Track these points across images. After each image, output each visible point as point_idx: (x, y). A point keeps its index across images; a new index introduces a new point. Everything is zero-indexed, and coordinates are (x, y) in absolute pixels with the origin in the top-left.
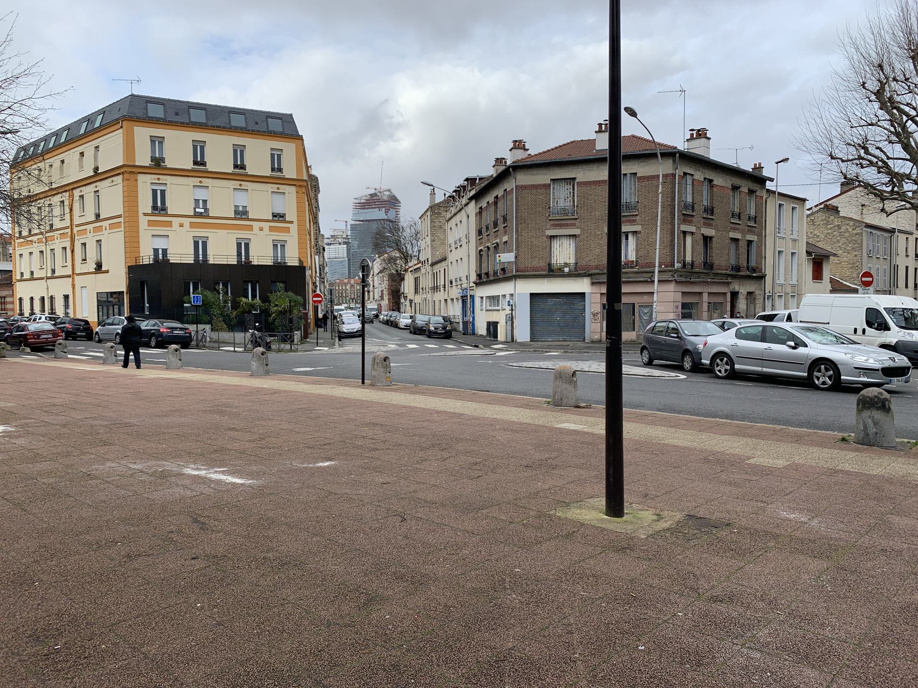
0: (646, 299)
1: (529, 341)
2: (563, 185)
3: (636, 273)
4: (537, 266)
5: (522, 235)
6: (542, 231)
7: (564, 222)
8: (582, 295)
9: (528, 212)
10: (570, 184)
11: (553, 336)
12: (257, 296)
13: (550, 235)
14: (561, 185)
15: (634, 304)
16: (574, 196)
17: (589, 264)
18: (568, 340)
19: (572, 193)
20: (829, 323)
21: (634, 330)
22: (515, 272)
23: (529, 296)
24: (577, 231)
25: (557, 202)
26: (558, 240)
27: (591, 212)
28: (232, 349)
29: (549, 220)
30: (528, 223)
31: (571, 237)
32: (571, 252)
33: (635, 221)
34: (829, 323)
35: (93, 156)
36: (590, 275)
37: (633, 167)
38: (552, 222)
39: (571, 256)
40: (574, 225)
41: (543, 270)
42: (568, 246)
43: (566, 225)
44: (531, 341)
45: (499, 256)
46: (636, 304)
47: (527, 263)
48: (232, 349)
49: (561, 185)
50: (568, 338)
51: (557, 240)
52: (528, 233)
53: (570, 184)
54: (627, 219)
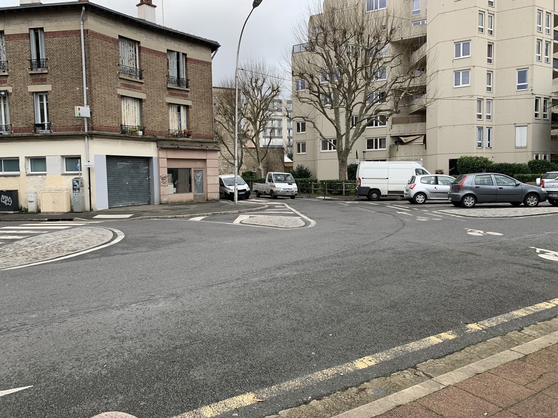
0: (199, 165)
1: (107, 208)
2: (127, 46)
3: (191, 142)
4: (111, 126)
5: (95, 89)
6: (114, 89)
7: (132, 84)
8: (148, 160)
9: (100, 64)
10: (133, 47)
11: (123, 201)
12: (431, 174)
13: (121, 94)
14: (125, 44)
15: (190, 169)
16: (136, 60)
17: (154, 130)
18: (136, 204)
19: (134, 56)
20: (387, 178)
21: (190, 191)
22: (88, 130)
23: (105, 159)
24: (143, 96)
25: (122, 61)
26: (125, 102)
27: (153, 80)
28: (323, 198)
29: (120, 78)
30: (100, 77)
31: (136, 100)
32: (137, 115)
33: (187, 96)
34: (387, 178)
35: (155, 23)
36: (157, 141)
37: (184, 48)
38: (122, 81)
39: (137, 119)
40: (140, 89)
41: (116, 131)
42: (134, 109)
43: (134, 88)
44: (109, 208)
45: (79, 109)
46: (192, 169)
47: (101, 121)
48: (323, 198)
49: (125, 44)
50: (136, 202)
51: (124, 101)
52: (101, 87)
53: (133, 47)
54: (182, 93)
